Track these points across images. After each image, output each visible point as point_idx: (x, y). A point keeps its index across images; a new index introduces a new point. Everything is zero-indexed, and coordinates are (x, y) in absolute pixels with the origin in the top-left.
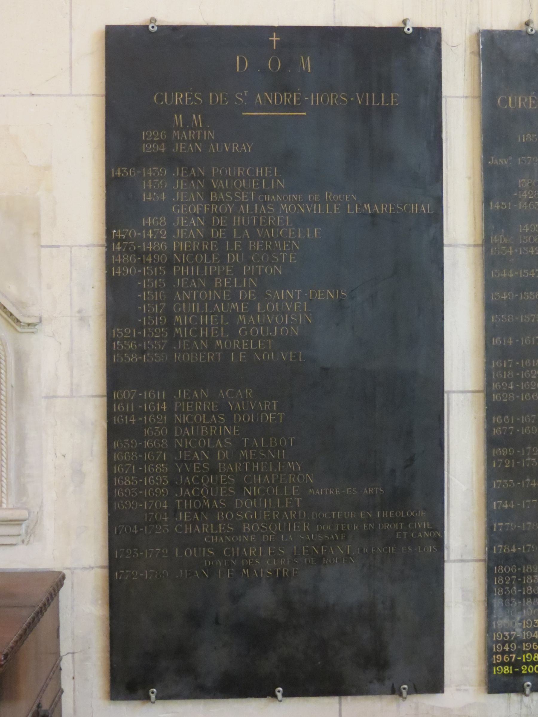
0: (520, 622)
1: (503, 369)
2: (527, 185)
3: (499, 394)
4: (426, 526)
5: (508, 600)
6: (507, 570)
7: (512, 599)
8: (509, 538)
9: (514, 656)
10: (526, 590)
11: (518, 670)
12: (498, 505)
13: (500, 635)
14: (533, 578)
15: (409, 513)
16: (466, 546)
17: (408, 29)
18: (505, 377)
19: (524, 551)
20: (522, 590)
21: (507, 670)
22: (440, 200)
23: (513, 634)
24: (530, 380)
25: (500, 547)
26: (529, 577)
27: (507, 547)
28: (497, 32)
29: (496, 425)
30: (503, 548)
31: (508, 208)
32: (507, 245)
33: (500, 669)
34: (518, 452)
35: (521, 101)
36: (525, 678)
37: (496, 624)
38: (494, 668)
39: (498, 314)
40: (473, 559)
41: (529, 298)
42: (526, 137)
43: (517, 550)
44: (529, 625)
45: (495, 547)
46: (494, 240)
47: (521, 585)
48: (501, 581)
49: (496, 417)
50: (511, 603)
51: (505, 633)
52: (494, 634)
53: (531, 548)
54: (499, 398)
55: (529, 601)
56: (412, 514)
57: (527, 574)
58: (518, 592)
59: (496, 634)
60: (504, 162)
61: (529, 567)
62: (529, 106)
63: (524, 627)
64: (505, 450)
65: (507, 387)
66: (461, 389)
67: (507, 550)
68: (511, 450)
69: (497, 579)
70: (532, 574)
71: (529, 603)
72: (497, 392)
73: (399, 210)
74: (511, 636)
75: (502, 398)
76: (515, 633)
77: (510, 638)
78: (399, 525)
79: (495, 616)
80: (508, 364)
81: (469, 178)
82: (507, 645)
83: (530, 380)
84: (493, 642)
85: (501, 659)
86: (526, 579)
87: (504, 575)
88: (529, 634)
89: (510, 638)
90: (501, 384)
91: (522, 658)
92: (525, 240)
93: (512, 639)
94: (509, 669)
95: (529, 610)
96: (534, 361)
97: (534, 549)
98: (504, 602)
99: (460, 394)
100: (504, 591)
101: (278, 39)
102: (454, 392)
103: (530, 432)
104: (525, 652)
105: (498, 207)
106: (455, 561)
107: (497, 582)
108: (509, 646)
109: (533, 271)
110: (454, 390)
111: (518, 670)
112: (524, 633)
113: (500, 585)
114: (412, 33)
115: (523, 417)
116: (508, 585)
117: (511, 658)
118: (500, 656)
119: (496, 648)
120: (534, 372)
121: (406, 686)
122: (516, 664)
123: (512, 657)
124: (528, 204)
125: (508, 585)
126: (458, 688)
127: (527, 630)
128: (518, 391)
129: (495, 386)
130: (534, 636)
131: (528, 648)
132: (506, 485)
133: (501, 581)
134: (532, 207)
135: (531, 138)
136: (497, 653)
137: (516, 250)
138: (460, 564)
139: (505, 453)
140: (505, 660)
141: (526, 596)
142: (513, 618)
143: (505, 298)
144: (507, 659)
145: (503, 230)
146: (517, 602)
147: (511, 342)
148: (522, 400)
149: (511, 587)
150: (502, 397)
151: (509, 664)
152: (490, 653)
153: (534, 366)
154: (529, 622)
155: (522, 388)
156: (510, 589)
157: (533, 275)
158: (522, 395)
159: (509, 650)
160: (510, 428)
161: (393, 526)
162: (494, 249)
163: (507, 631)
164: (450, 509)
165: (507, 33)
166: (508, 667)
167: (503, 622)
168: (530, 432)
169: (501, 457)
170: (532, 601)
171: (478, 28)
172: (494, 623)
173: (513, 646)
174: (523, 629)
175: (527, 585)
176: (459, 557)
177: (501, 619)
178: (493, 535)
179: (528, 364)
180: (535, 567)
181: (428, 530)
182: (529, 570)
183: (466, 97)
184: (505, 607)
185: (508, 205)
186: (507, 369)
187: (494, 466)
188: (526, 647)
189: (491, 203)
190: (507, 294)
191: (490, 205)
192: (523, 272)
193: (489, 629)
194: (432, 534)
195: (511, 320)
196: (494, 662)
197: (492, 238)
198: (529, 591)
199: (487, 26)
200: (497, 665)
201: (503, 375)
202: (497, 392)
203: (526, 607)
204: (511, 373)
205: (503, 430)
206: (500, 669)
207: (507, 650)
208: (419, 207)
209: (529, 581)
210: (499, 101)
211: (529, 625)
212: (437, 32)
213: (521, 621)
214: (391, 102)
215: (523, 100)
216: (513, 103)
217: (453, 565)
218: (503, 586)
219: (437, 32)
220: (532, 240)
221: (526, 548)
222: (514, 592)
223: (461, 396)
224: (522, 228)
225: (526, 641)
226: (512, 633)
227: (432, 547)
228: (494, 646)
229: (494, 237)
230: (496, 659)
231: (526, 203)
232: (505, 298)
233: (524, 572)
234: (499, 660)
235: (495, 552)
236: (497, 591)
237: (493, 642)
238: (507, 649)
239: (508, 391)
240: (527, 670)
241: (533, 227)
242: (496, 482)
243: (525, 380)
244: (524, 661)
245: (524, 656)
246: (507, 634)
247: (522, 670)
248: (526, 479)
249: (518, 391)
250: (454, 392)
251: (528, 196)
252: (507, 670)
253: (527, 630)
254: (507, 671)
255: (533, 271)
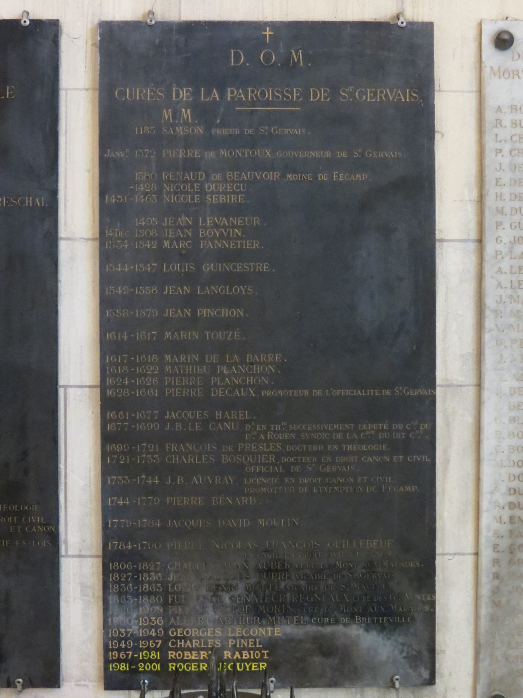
0: (136, 619)
1: (117, 365)
2: (144, 178)
3: (114, 390)
4: (40, 520)
5: (123, 596)
6: (123, 566)
7: (128, 596)
8: (125, 535)
9: (131, 653)
10: (142, 587)
11: (134, 667)
12: (112, 502)
13: (115, 632)
14: (150, 576)
15: (23, 507)
16: (84, 541)
17: (25, 22)
18: (119, 372)
19: (140, 548)
20: (138, 587)
21: (123, 667)
22: (54, 193)
23: (130, 631)
24: (145, 375)
25: (115, 544)
26: (146, 575)
27: (122, 544)
28: (116, 24)
29: (111, 421)
30: (119, 545)
31: (124, 200)
32: (123, 239)
33: (116, 665)
34: (133, 448)
35: (140, 93)
36: (142, 676)
37: (112, 621)
38: (111, 664)
39: (112, 309)
40: (91, 554)
41: (145, 293)
42: (143, 129)
43: (133, 547)
44: (146, 623)
45: (110, 544)
46: (109, 233)
47: (136, 582)
48: (116, 578)
49: (110, 413)
50: (127, 599)
51: (121, 630)
52: (110, 631)
53: (147, 546)
54: (113, 394)
55: (146, 599)
56: (26, 508)
57: (142, 572)
58: (134, 590)
59: (112, 631)
60: (120, 154)
61: (145, 564)
62: (147, 98)
63: (141, 624)
64: (120, 446)
65: (122, 382)
66: (78, 384)
67: (122, 547)
68: (126, 446)
69: (113, 576)
70: (149, 572)
71: (146, 601)
72: (111, 387)
73: (13, 203)
74: (127, 633)
75: (117, 394)
76: (131, 630)
77: (127, 635)
78: (13, 519)
79: (111, 613)
80: (122, 360)
81: (89, 171)
82: (123, 642)
83: (145, 375)
84: (109, 639)
85: (117, 656)
86: (142, 576)
87: (120, 571)
88: (146, 631)
89: (127, 635)
90: (115, 380)
91: (139, 656)
92: (141, 234)
93: (129, 636)
94: (126, 666)
95: (146, 608)
96: (149, 357)
97: (151, 547)
98: (120, 599)
99: (77, 389)
100: (120, 588)
101: (264, 33)
102: (71, 386)
103: (145, 428)
104: (142, 650)
105: (114, 200)
106: (73, 556)
107: (112, 579)
108: (125, 643)
109: (149, 265)
110: (71, 384)
111: (134, 667)
112: (141, 630)
113: (116, 582)
114: (30, 24)
115: (138, 413)
116: (123, 582)
117: (127, 655)
118: (116, 652)
119: (112, 645)
120: (149, 368)
121: (21, 680)
122: (133, 662)
123: (129, 654)
124: (144, 197)
125: (123, 582)
126: (78, 683)
127: (143, 627)
128: (132, 387)
129: (109, 381)
130: (151, 634)
131: (145, 645)
132: (120, 482)
133: (116, 578)
134: (148, 200)
135: (149, 130)
136: (113, 650)
137: (132, 244)
138: (77, 560)
139: (120, 450)
140: (121, 657)
141: (143, 594)
142: (129, 615)
143: (120, 292)
144: (123, 656)
145: (118, 224)
146: (133, 599)
147: (126, 337)
148: (138, 395)
149: (127, 583)
150: (116, 393)
151: (125, 661)
152: (106, 649)
153: (149, 361)
154: (146, 620)
155: (138, 384)
156: (126, 586)
157: (149, 269)
158: (137, 390)
159: (126, 647)
160: (125, 424)
161: (7, 520)
162: (109, 243)
163: (123, 628)
164: (68, 504)
165: (126, 23)
166: (124, 664)
167: (119, 619)
168: (145, 428)
169: (115, 453)
170: (149, 598)
171: (100, 19)
172: (110, 620)
173: (130, 643)
174: (140, 627)
175: (142, 583)
176: (77, 553)
177: (117, 616)
178: (107, 531)
179: (143, 359)
180: (152, 565)
181: (41, 524)
182: (145, 567)
183: (87, 89)
184: (120, 604)
185: (124, 198)
186: (122, 364)
187: (109, 462)
188: (143, 645)
189: (107, 197)
190: (122, 289)
191: (105, 198)
192: (138, 266)
193: (106, 625)
194: (46, 529)
195: (125, 315)
196: (110, 659)
197: (107, 231)
198: (146, 589)
199: (109, 17)
200: (113, 661)
201: (118, 370)
202: (111, 387)
203: (143, 605)
204: (126, 368)
205: (117, 427)
206: (116, 665)
207: (123, 647)
208: (33, 201)
209: (146, 578)
210: (116, 93)
211: (146, 623)
212: (55, 24)
213: (137, 618)
214: (6, 95)
215: (141, 92)
216: (131, 95)
217: (72, 560)
218: (119, 582)
219: (55, 24)
220: (148, 233)
221: (142, 546)
222: (130, 589)
223: (79, 391)
224: (138, 222)
225: (143, 639)
226: (128, 630)
227: (46, 542)
228: (110, 642)
229: (109, 230)
230: (112, 656)
231: (142, 197)
232: (120, 292)
233: (140, 569)
234: (115, 656)
235: (110, 548)
236: (113, 587)
237: (109, 639)
238: (123, 646)
239: (123, 386)
240: (144, 668)
241: (149, 220)
242: (111, 479)
243: (141, 375)
244: (141, 658)
245: (141, 653)
246: (123, 631)
247: (139, 668)
248: (141, 475)
249: (132, 387)
250: (71, 386)
251: (146, 189)
252: (123, 667)
253: (143, 627)
254: (123, 668)
255: (149, 265)
